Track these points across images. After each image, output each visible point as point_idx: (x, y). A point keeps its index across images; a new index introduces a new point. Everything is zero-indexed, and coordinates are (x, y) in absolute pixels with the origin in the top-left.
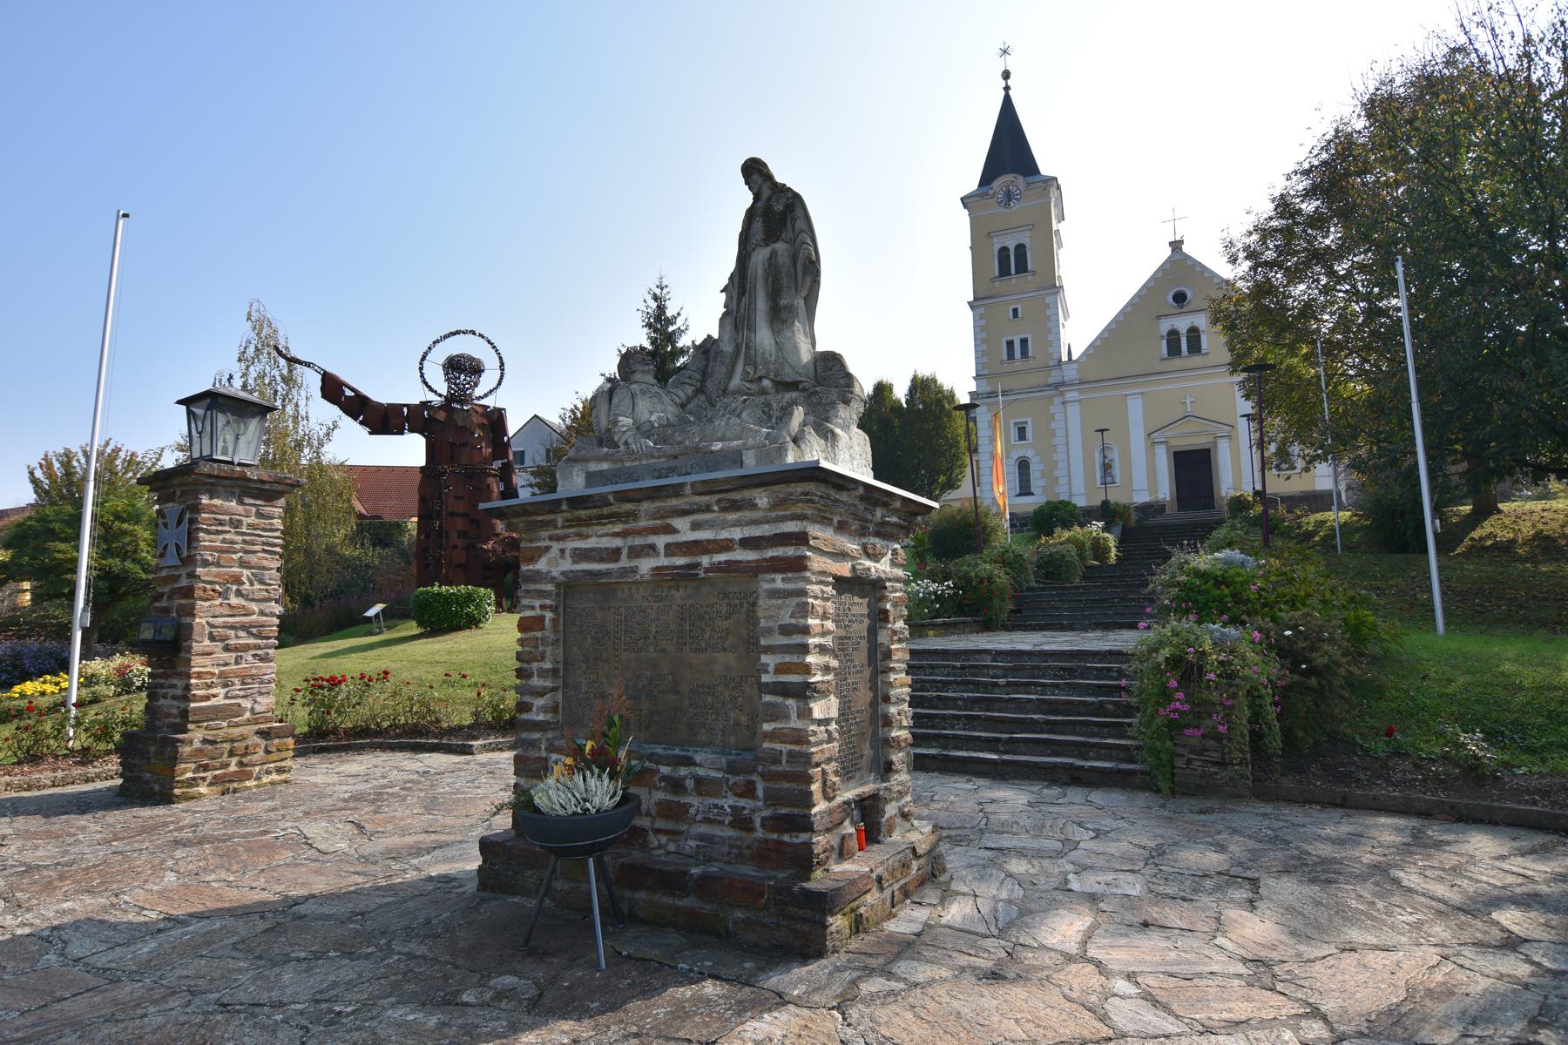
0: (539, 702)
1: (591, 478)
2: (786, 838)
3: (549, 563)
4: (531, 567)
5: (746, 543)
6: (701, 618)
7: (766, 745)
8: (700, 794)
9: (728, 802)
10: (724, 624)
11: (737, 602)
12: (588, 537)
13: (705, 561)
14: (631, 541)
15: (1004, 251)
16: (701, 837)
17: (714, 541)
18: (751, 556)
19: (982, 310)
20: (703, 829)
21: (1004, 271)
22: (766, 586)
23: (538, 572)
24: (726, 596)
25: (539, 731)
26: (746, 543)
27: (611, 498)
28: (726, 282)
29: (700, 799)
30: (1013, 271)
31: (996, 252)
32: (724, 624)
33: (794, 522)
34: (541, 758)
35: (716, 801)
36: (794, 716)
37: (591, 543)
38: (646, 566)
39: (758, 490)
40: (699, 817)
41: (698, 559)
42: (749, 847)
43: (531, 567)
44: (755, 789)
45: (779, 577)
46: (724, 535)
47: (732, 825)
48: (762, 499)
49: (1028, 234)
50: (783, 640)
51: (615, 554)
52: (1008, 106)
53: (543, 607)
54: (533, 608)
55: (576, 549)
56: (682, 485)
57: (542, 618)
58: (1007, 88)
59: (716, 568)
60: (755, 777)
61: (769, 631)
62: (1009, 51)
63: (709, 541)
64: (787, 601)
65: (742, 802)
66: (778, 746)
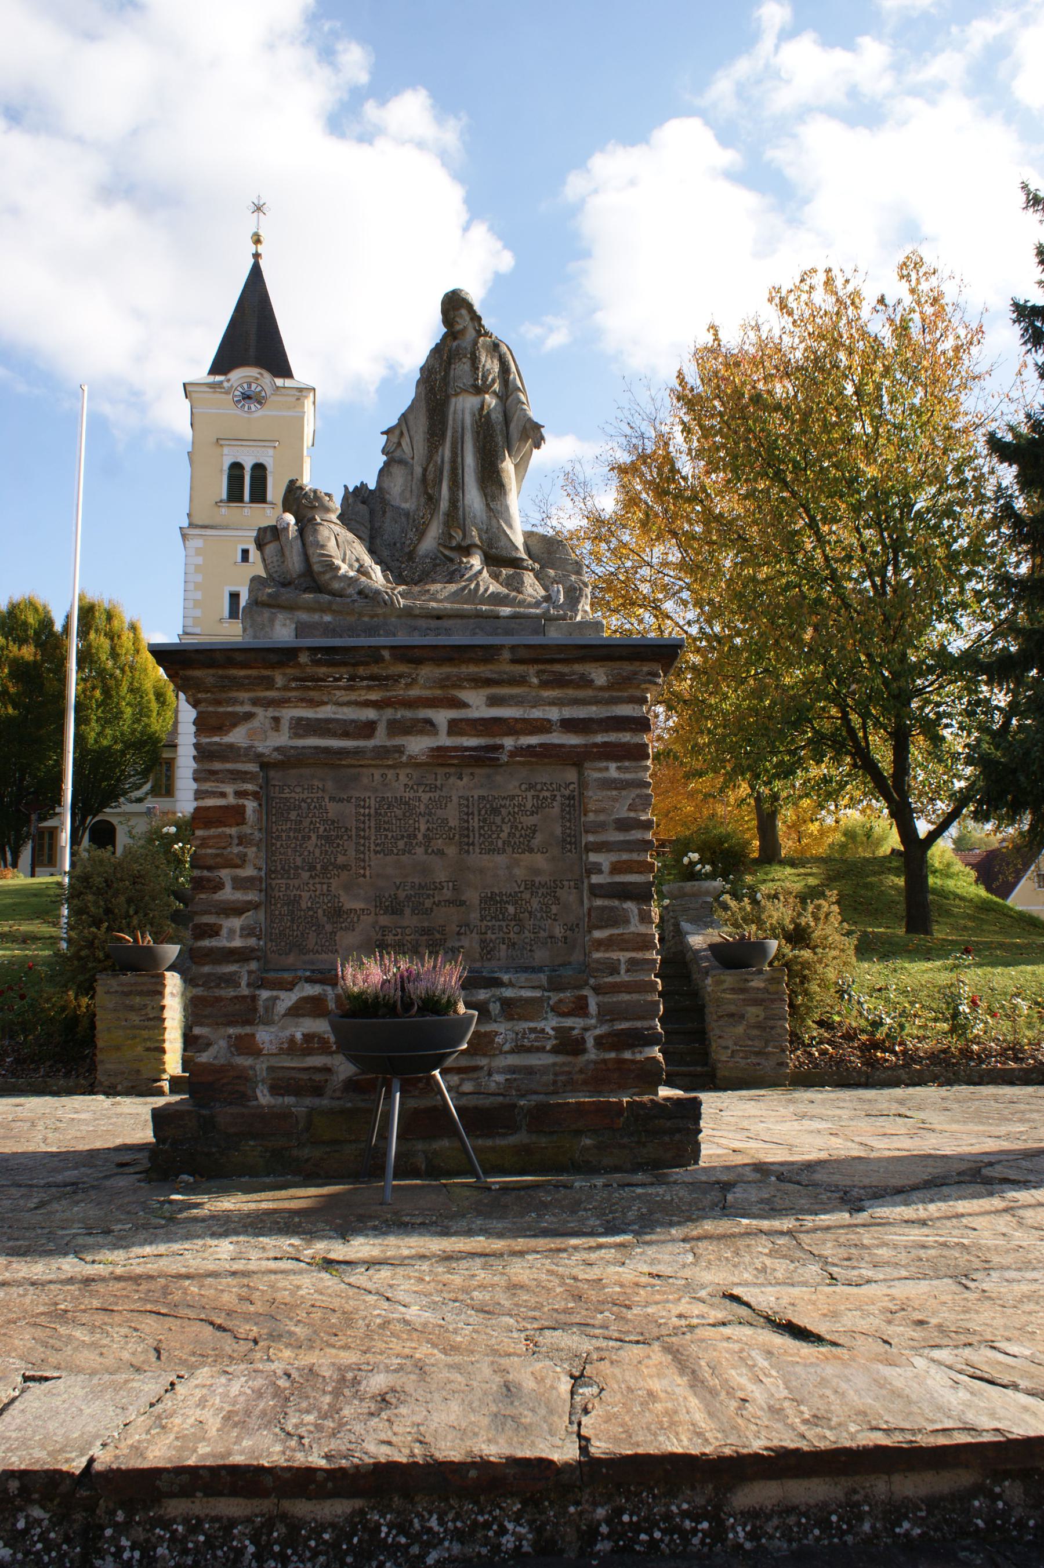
0: (236, 923)
1: (301, 630)
2: (627, 1055)
3: (250, 735)
4: (216, 739)
5: (569, 725)
6: (495, 811)
7: (597, 955)
8: (510, 1018)
9: (550, 1024)
10: (530, 820)
11: (547, 794)
12: (324, 703)
13: (509, 742)
14: (389, 713)
15: (236, 468)
16: (512, 1070)
17: (524, 720)
18: (573, 740)
19: (198, 543)
20: (512, 1060)
21: (235, 495)
22: (597, 775)
23: (231, 746)
24: (531, 787)
25: (237, 961)
26: (569, 725)
27: (386, 654)
28: (394, 422)
29: (509, 1025)
30: (247, 496)
31: (226, 467)
32: (530, 820)
33: (631, 706)
34: (244, 997)
35: (532, 1025)
36: (635, 919)
37: (326, 712)
38: (417, 745)
39: (594, 665)
40: (507, 1047)
41: (498, 741)
42: (581, 1071)
43: (216, 739)
44: (587, 1005)
45: (613, 766)
46: (536, 713)
47: (556, 1051)
48: (599, 675)
49: (271, 452)
50: (620, 837)
51: (368, 729)
52: (256, 277)
53: (239, 794)
54: (223, 795)
55: (300, 719)
56: (498, 648)
57: (240, 810)
58: (257, 256)
59: (519, 751)
60: (586, 992)
61: (600, 827)
62: (264, 209)
63: (516, 720)
64: (624, 793)
65: (569, 1022)
66: (614, 955)
